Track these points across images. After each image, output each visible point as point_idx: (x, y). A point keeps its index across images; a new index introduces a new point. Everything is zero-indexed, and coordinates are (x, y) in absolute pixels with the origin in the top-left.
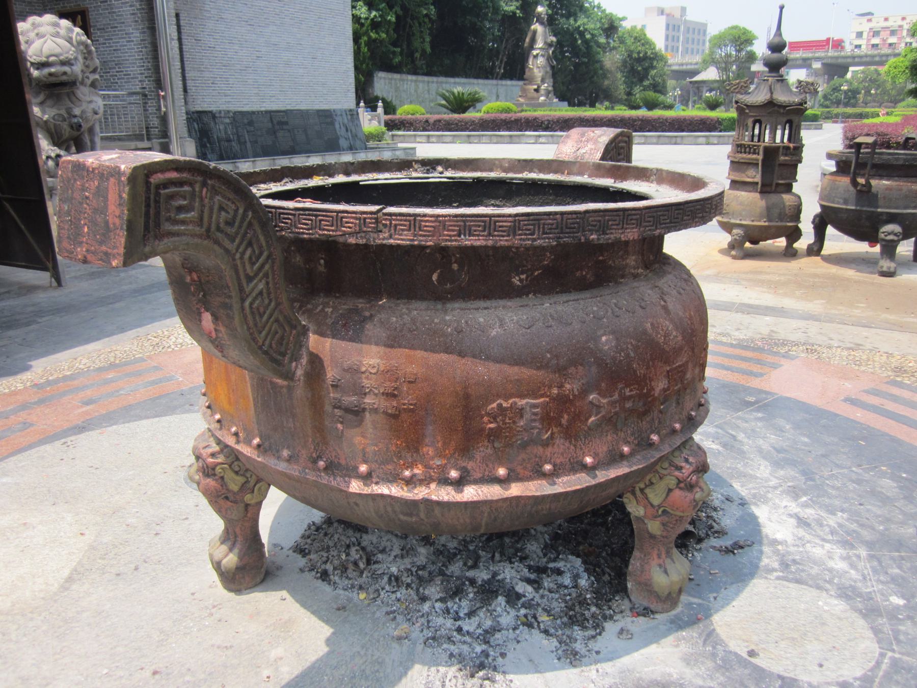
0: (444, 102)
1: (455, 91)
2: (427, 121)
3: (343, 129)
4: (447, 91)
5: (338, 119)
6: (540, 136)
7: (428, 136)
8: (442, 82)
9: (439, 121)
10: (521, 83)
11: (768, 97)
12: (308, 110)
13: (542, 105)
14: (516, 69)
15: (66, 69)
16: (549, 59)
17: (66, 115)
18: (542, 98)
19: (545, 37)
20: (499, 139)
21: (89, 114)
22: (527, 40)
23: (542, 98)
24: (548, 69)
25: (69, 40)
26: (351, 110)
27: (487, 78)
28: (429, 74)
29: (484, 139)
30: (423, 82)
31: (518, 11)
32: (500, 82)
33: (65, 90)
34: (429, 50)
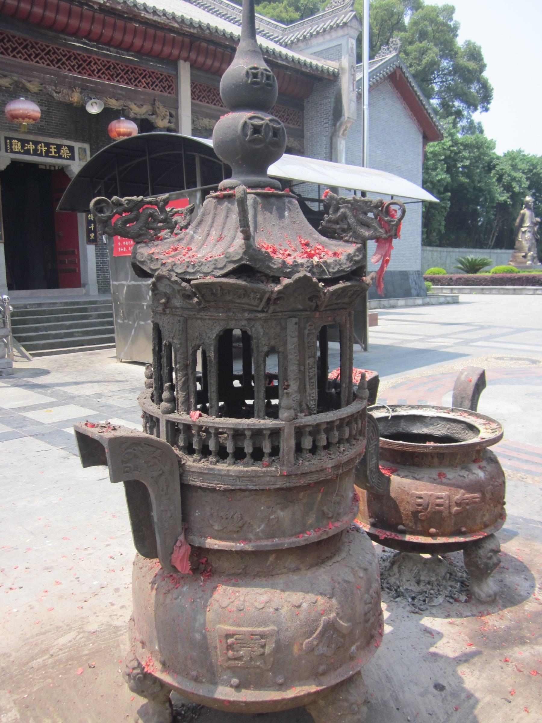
0: (460, 266)
1: (470, 259)
2: (451, 279)
3: (414, 283)
4: (464, 258)
5: (411, 277)
6: (537, 289)
7: (452, 289)
8: (450, 252)
9: (460, 279)
10: (511, 251)
11: (236, 246)
12: (394, 271)
13: (530, 267)
14: (507, 240)
16: (534, 234)
18: (529, 262)
19: (531, 218)
20: (506, 291)
22: (518, 221)
23: (529, 262)
24: (534, 241)
26: (418, 271)
27: (481, 248)
28: (440, 245)
29: (494, 291)
30: (437, 251)
31: (509, 200)
32: (492, 251)
34: (443, 231)
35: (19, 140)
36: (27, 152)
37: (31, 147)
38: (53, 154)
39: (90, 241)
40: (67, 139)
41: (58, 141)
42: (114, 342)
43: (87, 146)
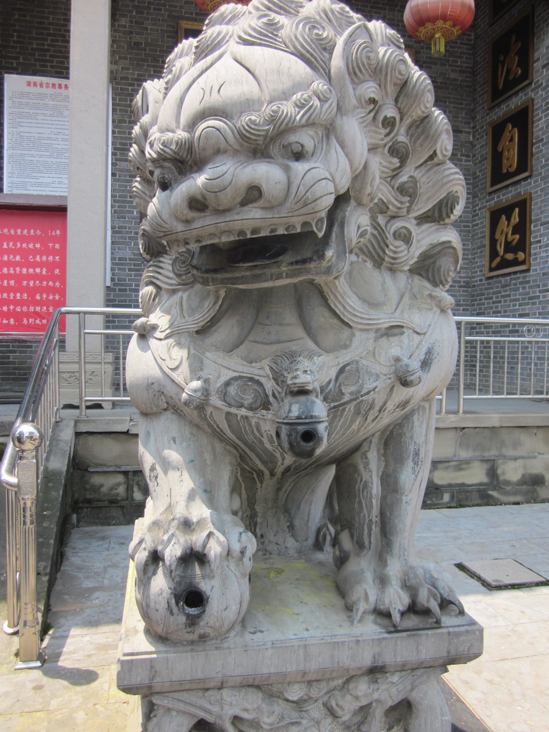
15: (267, 173)
17: (269, 385)
21: (376, 382)
25: (316, 55)
33: (280, 278)
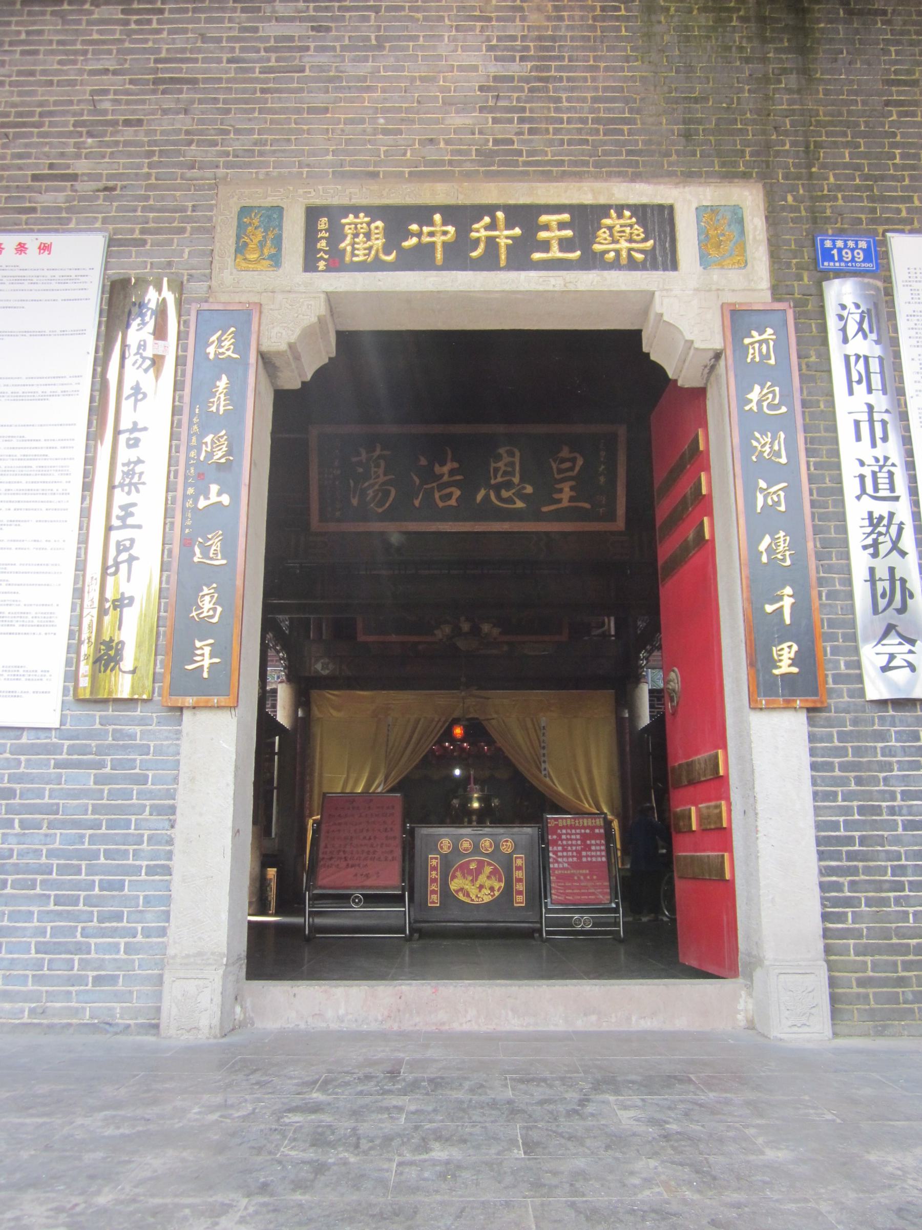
35: (374, 212)
36: (421, 259)
37: (441, 233)
38: (555, 253)
39: (770, 691)
40: (636, 177)
41: (584, 193)
42: (250, 922)
43: (749, 199)
